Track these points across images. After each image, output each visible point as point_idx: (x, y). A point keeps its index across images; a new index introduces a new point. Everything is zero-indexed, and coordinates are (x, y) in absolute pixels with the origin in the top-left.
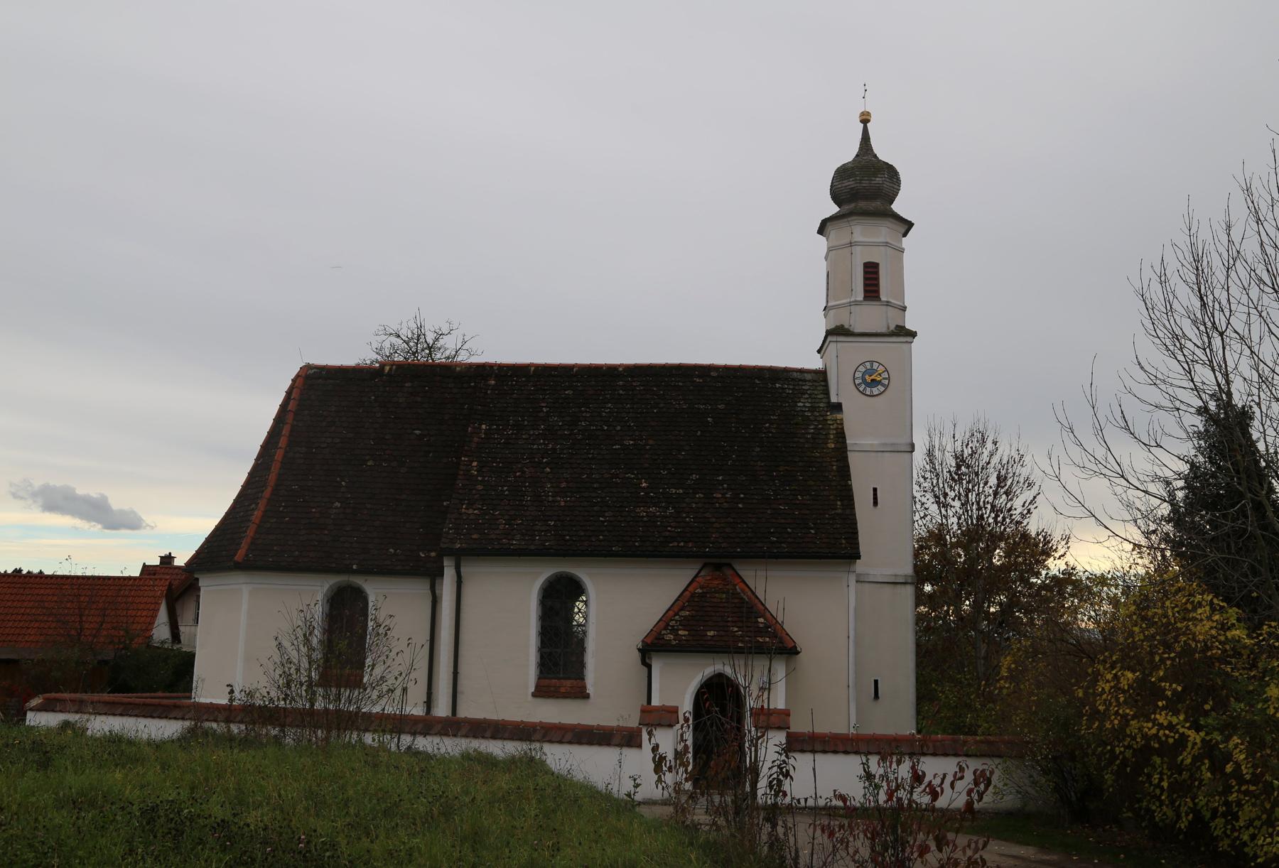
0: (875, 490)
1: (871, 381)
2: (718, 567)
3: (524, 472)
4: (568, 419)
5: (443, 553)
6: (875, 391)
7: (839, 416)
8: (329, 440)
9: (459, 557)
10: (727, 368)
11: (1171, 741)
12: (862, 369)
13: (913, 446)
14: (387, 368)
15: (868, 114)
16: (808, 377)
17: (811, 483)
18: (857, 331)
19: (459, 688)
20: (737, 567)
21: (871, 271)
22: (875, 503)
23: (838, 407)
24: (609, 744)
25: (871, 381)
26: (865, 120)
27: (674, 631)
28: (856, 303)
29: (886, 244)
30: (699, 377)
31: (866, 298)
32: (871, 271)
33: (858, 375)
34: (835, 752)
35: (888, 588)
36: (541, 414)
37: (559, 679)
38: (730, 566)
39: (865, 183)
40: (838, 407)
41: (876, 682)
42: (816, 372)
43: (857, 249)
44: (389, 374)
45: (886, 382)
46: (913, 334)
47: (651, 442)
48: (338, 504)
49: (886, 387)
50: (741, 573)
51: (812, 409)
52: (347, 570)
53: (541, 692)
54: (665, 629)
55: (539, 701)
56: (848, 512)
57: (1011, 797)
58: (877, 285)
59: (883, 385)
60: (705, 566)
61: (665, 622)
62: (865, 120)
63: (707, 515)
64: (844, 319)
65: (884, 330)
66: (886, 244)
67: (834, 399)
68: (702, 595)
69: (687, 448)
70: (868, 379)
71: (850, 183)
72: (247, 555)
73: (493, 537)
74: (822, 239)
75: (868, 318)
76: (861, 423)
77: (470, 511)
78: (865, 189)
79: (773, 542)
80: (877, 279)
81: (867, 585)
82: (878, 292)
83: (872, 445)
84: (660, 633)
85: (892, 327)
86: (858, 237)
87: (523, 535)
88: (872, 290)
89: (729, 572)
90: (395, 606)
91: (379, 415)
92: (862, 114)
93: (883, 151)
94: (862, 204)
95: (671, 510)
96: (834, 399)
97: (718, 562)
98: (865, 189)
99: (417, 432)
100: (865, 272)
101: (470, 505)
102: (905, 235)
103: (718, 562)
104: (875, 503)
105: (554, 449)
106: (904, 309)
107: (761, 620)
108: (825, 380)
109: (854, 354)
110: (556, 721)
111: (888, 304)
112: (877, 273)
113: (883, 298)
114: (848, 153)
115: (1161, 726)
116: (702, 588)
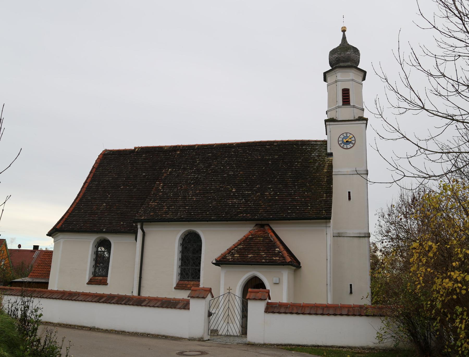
0: (349, 193)
1: (347, 142)
2: (262, 226)
3: (182, 187)
4: (207, 165)
5: (136, 221)
6: (349, 146)
7: (331, 158)
8: (107, 179)
9: (142, 222)
10: (282, 142)
11: (464, 292)
12: (342, 136)
13: (367, 171)
14: (137, 149)
15: (345, 27)
16: (319, 143)
17: (313, 187)
18: (339, 120)
19: (142, 284)
20: (271, 226)
21: (346, 93)
22: (350, 199)
23: (331, 154)
24: (175, 308)
25: (347, 142)
26: (344, 31)
27: (233, 255)
28: (339, 107)
29: (353, 80)
30: (268, 145)
31: (343, 104)
32: (346, 93)
33: (340, 139)
34: (291, 313)
35: (356, 240)
36: (196, 164)
37: (188, 281)
38: (268, 225)
39: (343, 55)
40: (331, 154)
41: (351, 285)
42: (323, 141)
43: (339, 83)
44: (137, 152)
45: (354, 142)
46: (366, 120)
47: (241, 173)
48: (105, 204)
49: (354, 144)
50: (274, 229)
51: (319, 156)
52: (101, 232)
53: (179, 287)
54: (229, 254)
55: (178, 291)
56: (329, 198)
57: (390, 340)
58: (349, 99)
59: (352, 143)
60: (257, 225)
61: (230, 251)
62: (344, 31)
63: (260, 202)
64: (333, 115)
65: (352, 119)
66: (353, 80)
67: (329, 151)
68: (251, 239)
69: (257, 174)
70: (345, 141)
71: (336, 55)
72: (62, 226)
73: (159, 214)
74: (326, 83)
75: (346, 113)
76: (341, 162)
77: (153, 204)
78: (344, 58)
79: (289, 213)
80: (349, 96)
81: (346, 238)
82: (349, 101)
83: (347, 171)
84: (225, 256)
85: (357, 117)
86: (339, 78)
87: (173, 213)
88: (346, 99)
89: (267, 228)
90: (123, 251)
91: (130, 168)
92: (342, 28)
93: (351, 42)
94: (342, 64)
95: (244, 200)
96: (329, 151)
97: (263, 223)
98: (344, 58)
99: (144, 174)
100: (343, 93)
101: (154, 201)
102: (364, 79)
103: (263, 223)
104: (350, 199)
105: (197, 177)
106: (363, 110)
107: (278, 249)
108: (326, 144)
109: (338, 129)
110: (155, 296)
111: (354, 107)
112: (349, 93)
113: (351, 104)
114: (337, 43)
115: (456, 281)
116: (252, 235)
